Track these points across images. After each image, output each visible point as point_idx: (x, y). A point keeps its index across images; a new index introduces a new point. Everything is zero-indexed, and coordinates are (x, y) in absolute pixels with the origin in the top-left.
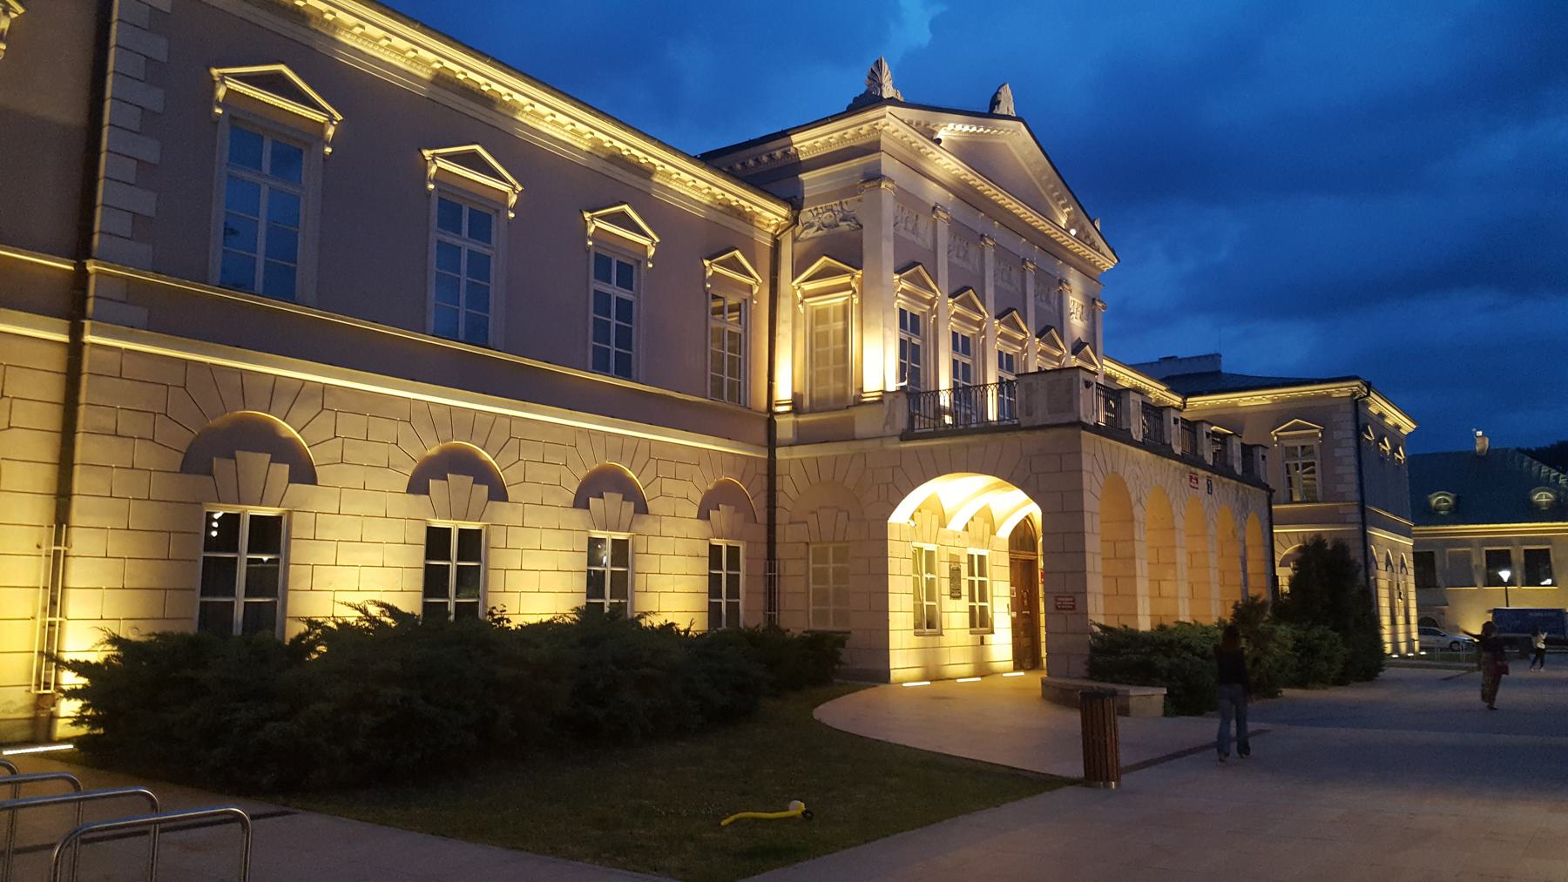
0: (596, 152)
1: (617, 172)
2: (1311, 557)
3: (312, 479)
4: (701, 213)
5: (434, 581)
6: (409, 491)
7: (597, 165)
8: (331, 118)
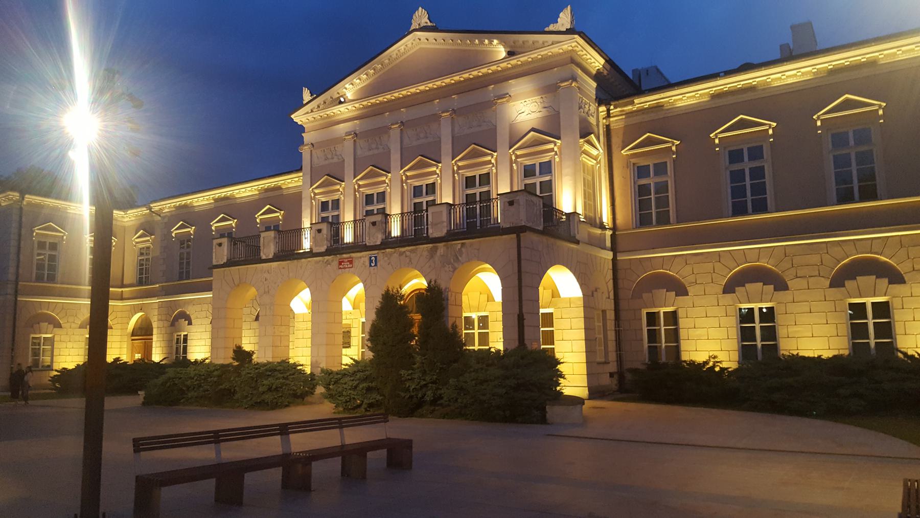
2: (389, 315)
3: (785, 287)
5: (858, 331)
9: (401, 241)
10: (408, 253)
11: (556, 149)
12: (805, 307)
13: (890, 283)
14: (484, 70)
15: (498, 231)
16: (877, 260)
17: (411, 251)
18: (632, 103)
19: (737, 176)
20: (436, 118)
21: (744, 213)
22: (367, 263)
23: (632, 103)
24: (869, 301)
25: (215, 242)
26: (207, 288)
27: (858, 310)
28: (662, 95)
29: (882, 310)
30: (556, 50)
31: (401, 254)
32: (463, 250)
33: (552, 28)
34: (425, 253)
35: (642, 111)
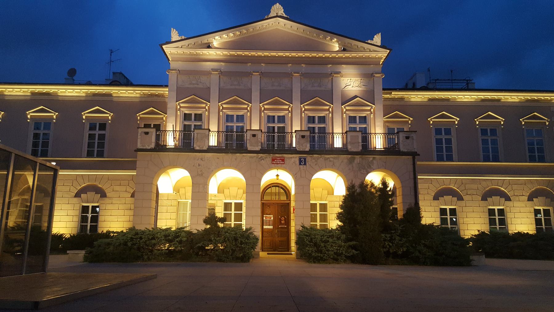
0: (87, 95)
1: (150, 99)
4: (137, 100)
5: (492, 222)
6: (528, 201)
7: (89, 98)
8: (410, 119)
9: (176, 149)
10: (331, 159)
11: (207, 108)
12: (470, 209)
13: (506, 200)
14: (321, 55)
15: (294, 151)
16: (499, 189)
17: (334, 158)
18: (391, 94)
19: (439, 142)
20: (289, 75)
21: (442, 160)
22: (298, 162)
23: (391, 94)
24: (448, 207)
25: (140, 130)
26: (131, 166)
27: (491, 212)
28: (407, 93)
29: (501, 212)
30: (373, 55)
31: (326, 159)
32: (374, 161)
33: (369, 41)
34: (346, 161)
35: (393, 99)
